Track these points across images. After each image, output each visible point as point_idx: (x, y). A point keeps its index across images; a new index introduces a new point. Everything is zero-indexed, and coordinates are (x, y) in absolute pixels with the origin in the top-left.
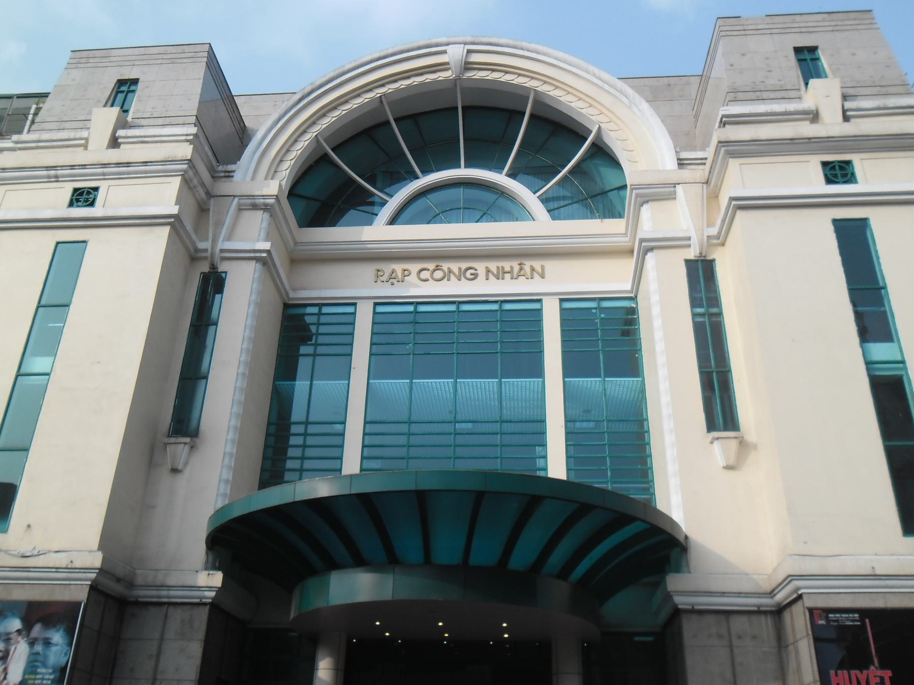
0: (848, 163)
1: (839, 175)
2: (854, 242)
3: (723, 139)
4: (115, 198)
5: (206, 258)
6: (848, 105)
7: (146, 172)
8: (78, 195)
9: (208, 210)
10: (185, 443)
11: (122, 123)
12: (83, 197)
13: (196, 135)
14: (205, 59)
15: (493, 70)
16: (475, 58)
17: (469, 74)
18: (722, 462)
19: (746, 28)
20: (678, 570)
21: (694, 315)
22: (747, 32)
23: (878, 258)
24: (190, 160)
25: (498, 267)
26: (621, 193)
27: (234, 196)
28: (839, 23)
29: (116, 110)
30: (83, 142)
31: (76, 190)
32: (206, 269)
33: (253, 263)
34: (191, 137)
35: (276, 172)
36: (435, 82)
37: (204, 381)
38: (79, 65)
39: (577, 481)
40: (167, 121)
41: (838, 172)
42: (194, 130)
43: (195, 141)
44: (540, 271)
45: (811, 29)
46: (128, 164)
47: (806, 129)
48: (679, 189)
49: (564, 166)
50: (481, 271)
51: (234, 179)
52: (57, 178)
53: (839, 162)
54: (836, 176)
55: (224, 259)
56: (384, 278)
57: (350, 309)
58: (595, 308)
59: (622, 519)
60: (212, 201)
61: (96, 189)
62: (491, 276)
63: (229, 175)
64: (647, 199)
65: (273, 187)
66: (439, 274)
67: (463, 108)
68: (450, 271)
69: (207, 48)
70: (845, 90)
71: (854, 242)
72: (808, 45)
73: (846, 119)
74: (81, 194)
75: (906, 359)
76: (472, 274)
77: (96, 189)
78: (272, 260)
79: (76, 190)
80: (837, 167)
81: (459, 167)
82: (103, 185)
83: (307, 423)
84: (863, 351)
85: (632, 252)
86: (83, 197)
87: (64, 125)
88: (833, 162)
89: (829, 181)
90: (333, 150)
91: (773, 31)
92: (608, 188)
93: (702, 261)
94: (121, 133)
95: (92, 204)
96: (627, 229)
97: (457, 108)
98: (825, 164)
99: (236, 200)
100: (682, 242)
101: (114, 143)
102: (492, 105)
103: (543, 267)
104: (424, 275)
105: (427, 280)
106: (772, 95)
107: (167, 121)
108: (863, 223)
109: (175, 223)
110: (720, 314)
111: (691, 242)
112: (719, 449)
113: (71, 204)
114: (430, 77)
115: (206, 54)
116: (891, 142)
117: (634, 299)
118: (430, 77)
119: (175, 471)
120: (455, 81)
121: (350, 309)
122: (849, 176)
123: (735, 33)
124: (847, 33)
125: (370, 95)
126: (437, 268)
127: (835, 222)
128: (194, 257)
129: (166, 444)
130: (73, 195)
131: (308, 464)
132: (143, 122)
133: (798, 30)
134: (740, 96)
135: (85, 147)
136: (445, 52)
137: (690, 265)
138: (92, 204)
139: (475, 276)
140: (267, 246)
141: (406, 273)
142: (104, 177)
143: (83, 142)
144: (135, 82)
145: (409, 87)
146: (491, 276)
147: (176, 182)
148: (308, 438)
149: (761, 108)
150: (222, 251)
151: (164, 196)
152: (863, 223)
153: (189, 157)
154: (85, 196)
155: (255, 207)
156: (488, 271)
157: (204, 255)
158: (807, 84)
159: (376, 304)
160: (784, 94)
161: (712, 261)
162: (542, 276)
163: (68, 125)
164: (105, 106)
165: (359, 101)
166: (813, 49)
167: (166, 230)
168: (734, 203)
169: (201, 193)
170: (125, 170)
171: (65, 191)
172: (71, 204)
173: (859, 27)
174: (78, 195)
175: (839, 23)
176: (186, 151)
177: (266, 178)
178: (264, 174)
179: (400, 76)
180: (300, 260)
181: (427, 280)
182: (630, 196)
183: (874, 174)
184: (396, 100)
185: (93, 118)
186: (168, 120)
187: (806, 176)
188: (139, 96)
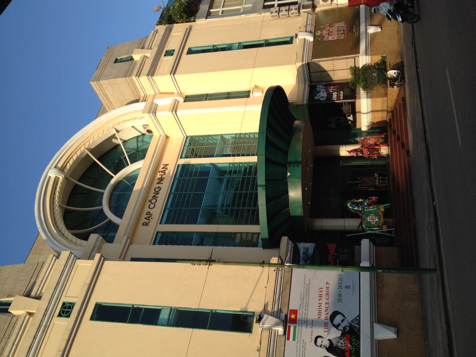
0: (64, 304)
2: (105, 313)
6: (33, 294)
7: (66, 276)
15: (68, 162)
16: (60, 165)
33: (177, 113)
41: (66, 310)
47: (34, 323)
48: (155, 101)
53: (61, 308)
56: (147, 221)
59: (268, 141)
66: (154, 201)
68: (154, 196)
71: (105, 313)
75: (238, 42)
89: (68, 316)
98: (60, 315)
104: (152, 206)
105: (155, 205)
111: (178, 99)
116: (166, 36)
120: (66, 179)
122: (70, 305)
127: (92, 319)
132: (33, 281)
141: (149, 213)
158: (10, 313)
160: (130, 71)
162: (167, 165)
179: (52, 196)
187: (61, 326)
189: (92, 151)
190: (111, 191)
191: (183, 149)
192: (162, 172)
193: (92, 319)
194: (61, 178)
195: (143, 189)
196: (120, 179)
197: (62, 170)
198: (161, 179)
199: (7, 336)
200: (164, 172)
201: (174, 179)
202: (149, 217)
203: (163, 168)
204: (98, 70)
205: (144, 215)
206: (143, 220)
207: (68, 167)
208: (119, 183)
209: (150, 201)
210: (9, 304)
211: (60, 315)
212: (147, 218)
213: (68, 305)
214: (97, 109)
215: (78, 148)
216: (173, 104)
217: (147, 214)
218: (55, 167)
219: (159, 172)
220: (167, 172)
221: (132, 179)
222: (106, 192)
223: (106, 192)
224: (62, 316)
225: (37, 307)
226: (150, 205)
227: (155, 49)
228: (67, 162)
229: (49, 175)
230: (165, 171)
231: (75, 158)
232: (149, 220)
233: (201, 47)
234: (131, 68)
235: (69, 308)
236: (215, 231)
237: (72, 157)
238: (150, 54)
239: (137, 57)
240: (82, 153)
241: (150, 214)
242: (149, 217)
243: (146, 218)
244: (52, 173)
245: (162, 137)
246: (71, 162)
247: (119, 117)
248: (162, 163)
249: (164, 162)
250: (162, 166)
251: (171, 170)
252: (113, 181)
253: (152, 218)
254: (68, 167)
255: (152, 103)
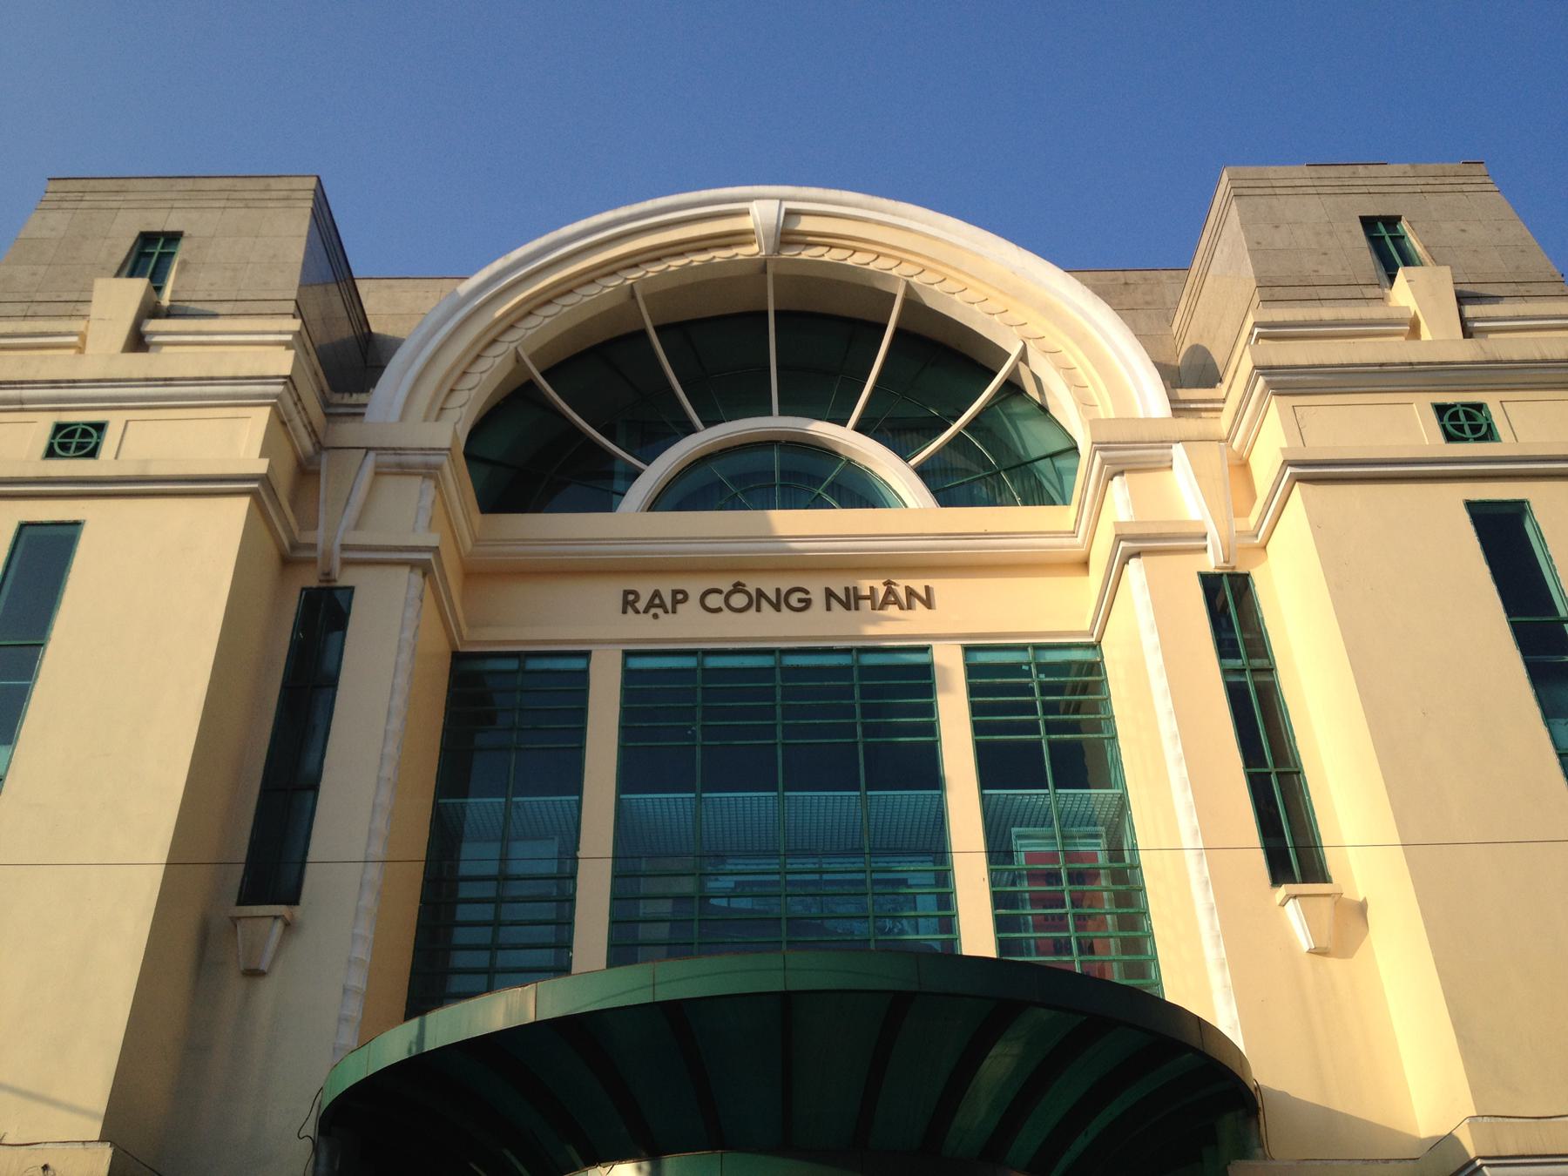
0: (1479, 407)
1: (1467, 428)
3: (1262, 363)
4: (136, 442)
5: (313, 561)
6: (1470, 311)
8: (64, 436)
9: (317, 473)
10: (276, 917)
11: (151, 310)
12: (75, 440)
13: (297, 334)
14: (310, 204)
16: (805, 224)
17: (788, 254)
18: (1304, 942)
19: (1275, 183)
20: (1244, 1152)
21: (1225, 672)
22: (1278, 191)
23: (1553, 569)
24: (289, 377)
25: (847, 589)
26: (1061, 463)
27: (368, 449)
28: (1431, 181)
29: (140, 285)
30: (74, 339)
31: (59, 427)
32: (313, 582)
34: (289, 338)
35: (442, 409)
36: (731, 262)
37: (310, 794)
38: (65, 205)
39: (1125, 982)
40: (241, 308)
41: (1463, 423)
42: (296, 324)
43: (300, 342)
44: (924, 595)
45: (1386, 189)
46: (168, 381)
47: (1394, 350)
48: (1178, 451)
49: (956, 419)
50: (818, 597)
51: (367, 418)
52: (21, 406)
54: (1460, 428)
55: (346, 563)
56: (641, 605)
57: (578, 664)
58: (1029, 664)
60: (325, 457)
61: (100, 427)
62: (834, 603)
63: (357, 413)
64: (1120, 468)
65: (448, 432)
66: (739, 600)
67: (777, 313)
69: (312, 183)
70: (1459, 287)
71: (1504, 537)
72: (1384, 213)
73: (1467, 333)
74: (71, 435)
76: (800, 600)
77: (100, 427)
78: (441, 565)
79: (59, 427)
80: (1462, 416)
81: (770, 414)
82: (115, 420)
83: (503, 878)
84: (1550, 731)
85: (1084, 564)
86: (75, 440)
87: (35, 308)
88: (1454, 406)
89: (1450, 438)
90: (657, 329)
91: (1320, 190)
92: (1034, 454)
93: (1229, 575)
94: (152, 325)
95: (92, 454)
96: (1077, 522)
97: (766, 313)
98: (1440, 409)
99: (372, 455)
100: (1193, 542)
101: (138, 342)
102: (818, 309)
103: (927, 589)
104: (714, 601)
105: (719, 610)
106: (1333, 293)
107: (241, 308)
108: (1518, 510)
109: (260, 491)
110: (1270, 670)
111: (1209, 542)
112: (1293, 914)
113: (50, 453)
114: (721, 255)
115: (311, 195)
117: (1095, 647)
118: (721, 255)
119: (254, 974)
121: (578, 664)
122: (1484, 429)
123: (1258, 191)
124: (1447, 197)
125: (615, 282)
126: (738, 588)
127: (1471, 506)
128: (288, 561)
129: (235, 920)
130: (54, 436)
131: (503, 958)
133: (1364, 189)
134: (1279, 293)
135: (80, 349)
136: (746, 213)
137: (1210, 583)
138: (92, 454)
139: (807, 604)
140: (433, 540)
142: (119, 403)
143: (74, 339)
144: (174, 238)
145: (707, 264)
146: (834, 603)
147: (262, 416)
148: (505, 908)
149: (1327, 313)
150: (344, 548)
151: (240, 441)
152: (1518, 510)
153: (288, 372)
154: (76, 439)
155: (404, 470)
156: (830, 594)
157: (312, 554)
159: (627, 654)
161: (1246, 577)
162: (928, 603)
163: (42, 309)
164: (118, 275)
165: (593, 290)
166: (1392, 222)
167: (244, 503)
168: (1289, 470)
169: (307, 444)
170: (171, 395)
171: (41, 428)
172: (50, 453)
173: (1465, 188)
174: (64, 436)
175: (1431, 181)
176: (282, 362)
177: (426, 419)
178: (422, 414)
180: (482, 574)
181: (719, 610)
182: (1087, 467)
183: (1526, 423)
184: (663, 294)
185: (97, 296)
186: (244, 307)
187: (1412, 427)
188: (184, 265)
189: (913, 304)
190: (784, 439)
191: (1023, 648)
192: (889, 592)
193: (1471, 506)
194: (755, 249)
195: (780, 546)
196: (841, 451)
197: (787, 236)
198: (851, 600)
199: (1522, 289)
200: (890, 598)
201: (848, 651)
202: (662, 605)
203: (910, 593)
204: (1312, 172)
205: (666, 587)
206: (645, 588)
207: (807, 254)
208: (825, 453)
209: (738, 588)
210: (1408, 261)
211: (1440, 409)
212: (656, 601)
213: (1481, 420)
214: (1128, 250)
215: (901, 255)
216: (1186, 530)
217: (675, 592)
218: (790, 213)
219: (888, 583)
220: (893, 610)
221: (858, 490)
222: (776, 423)
223: (776, 423)
224: (1440, 416)
225: (1439, 338)
226: (720, 592)
227: (1466, 351)
228: (829, 240)
229: (754, 207)
230: (897, 602)
231: (856, 260)
232: (650, 605)
233: (1549, 559)
234: (1324, 292)
235: (1475, 429)
236: (606, 867)
237: (831, 247)
238: (1439, 338)
239: (1403, 293)
240: (884, 276)
241: (675, 602)
242: (662, 605)
243: (657, 594)
244: (761, 210)
245: (1066, 541)
246: (833, 256)
247: (1082, 340)
248: (930, 582)
249: (942, 587)
250: (918, 585)
251: (893, 626)
252: (822, 429)
253: (656, 616)
254: (807, 254)
255: (1166, 443)
